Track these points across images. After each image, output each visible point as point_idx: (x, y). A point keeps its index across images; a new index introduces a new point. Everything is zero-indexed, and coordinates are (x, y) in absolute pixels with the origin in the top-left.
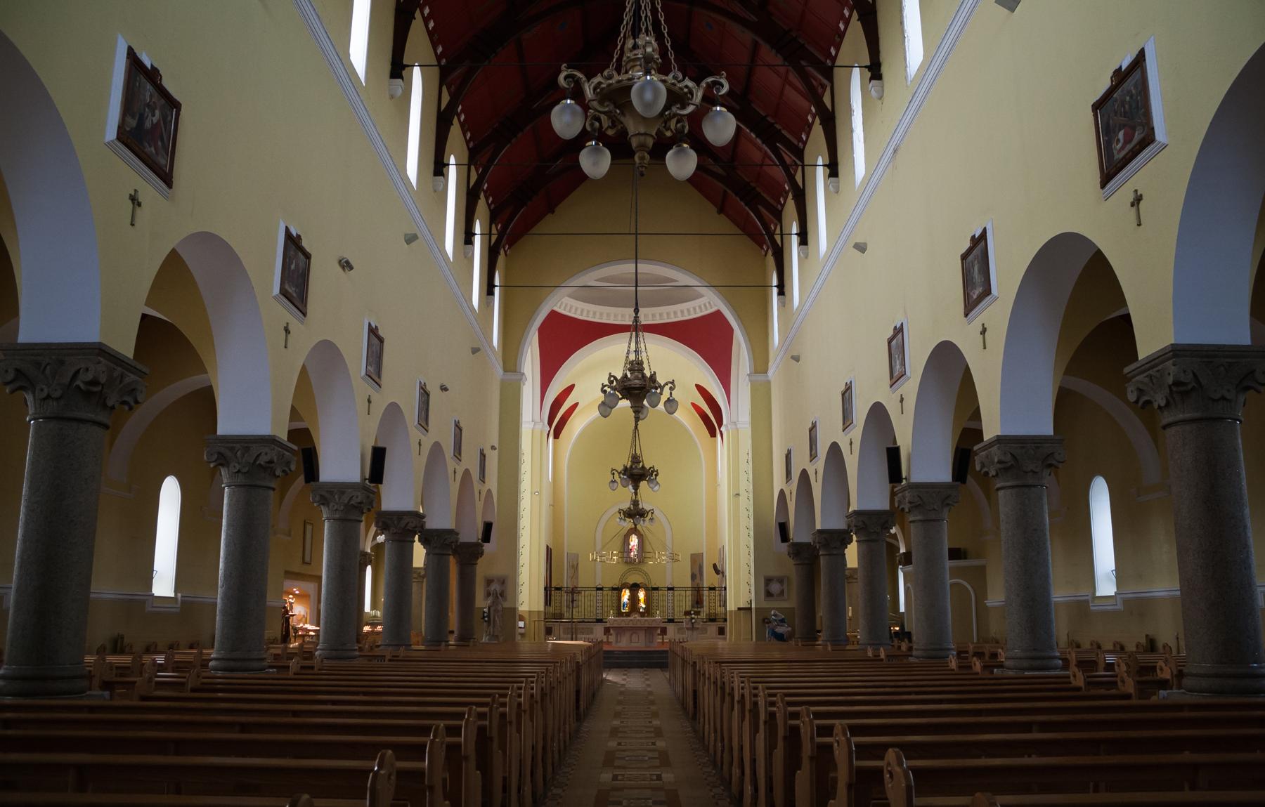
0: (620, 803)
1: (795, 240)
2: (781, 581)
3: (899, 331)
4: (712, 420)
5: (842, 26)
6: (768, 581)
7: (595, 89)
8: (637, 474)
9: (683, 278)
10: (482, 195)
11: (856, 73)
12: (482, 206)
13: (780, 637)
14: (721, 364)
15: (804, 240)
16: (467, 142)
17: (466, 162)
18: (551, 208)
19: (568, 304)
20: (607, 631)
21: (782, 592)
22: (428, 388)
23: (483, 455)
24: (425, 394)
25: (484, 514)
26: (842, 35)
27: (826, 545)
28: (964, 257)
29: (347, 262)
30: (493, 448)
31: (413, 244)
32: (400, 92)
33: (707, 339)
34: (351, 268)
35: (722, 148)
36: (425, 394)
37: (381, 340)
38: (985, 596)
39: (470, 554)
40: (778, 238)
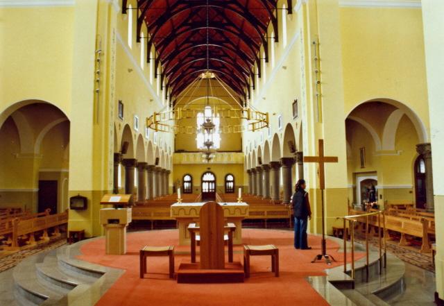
1: (273, 40)
3: (296, 102)
10: (144, 21)
12: (144, 26)
15: (276, 39)
17: (136, 7)
27: (258, 170)
40: (266, 39)
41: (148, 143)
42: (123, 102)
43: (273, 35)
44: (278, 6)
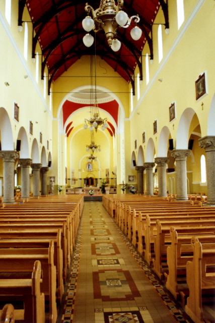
0: (99, 249)
2: (133, 177)
3: (173, 105)
4: (112, 131)
5: (156, 12)
6: (129, 177)
7: (96, 14)
8: (93, 147)
9: (105, 90)
11: (160, 26)
12: (38, 47)
13: (133, 193)
14: (115, 115)
15: (141, 78)
16: (41, 48)
18: (66, 69)
19: (70, 97)
20: (83, 191)
21: (133, 180)
22: (32, 122)
23: (48, 142)
24: (31, 124)
25: (49, 159)
26: (155, 15)
28: (197, 82)
29: (7, 83)
30: (51, 140)
31: (27, 79)
32: (21, 30)
33: (112, 108)
34: (8, 85)
35: (138, 41)
36: (31, 124)
37: (18, 108)
38: (192, 181)
39: (44, 171)
40: (133, 78)
41: (42, 147)
42: (18, 105)
43: (138, 75)
44: (143, 54)
